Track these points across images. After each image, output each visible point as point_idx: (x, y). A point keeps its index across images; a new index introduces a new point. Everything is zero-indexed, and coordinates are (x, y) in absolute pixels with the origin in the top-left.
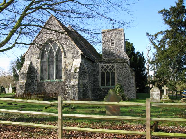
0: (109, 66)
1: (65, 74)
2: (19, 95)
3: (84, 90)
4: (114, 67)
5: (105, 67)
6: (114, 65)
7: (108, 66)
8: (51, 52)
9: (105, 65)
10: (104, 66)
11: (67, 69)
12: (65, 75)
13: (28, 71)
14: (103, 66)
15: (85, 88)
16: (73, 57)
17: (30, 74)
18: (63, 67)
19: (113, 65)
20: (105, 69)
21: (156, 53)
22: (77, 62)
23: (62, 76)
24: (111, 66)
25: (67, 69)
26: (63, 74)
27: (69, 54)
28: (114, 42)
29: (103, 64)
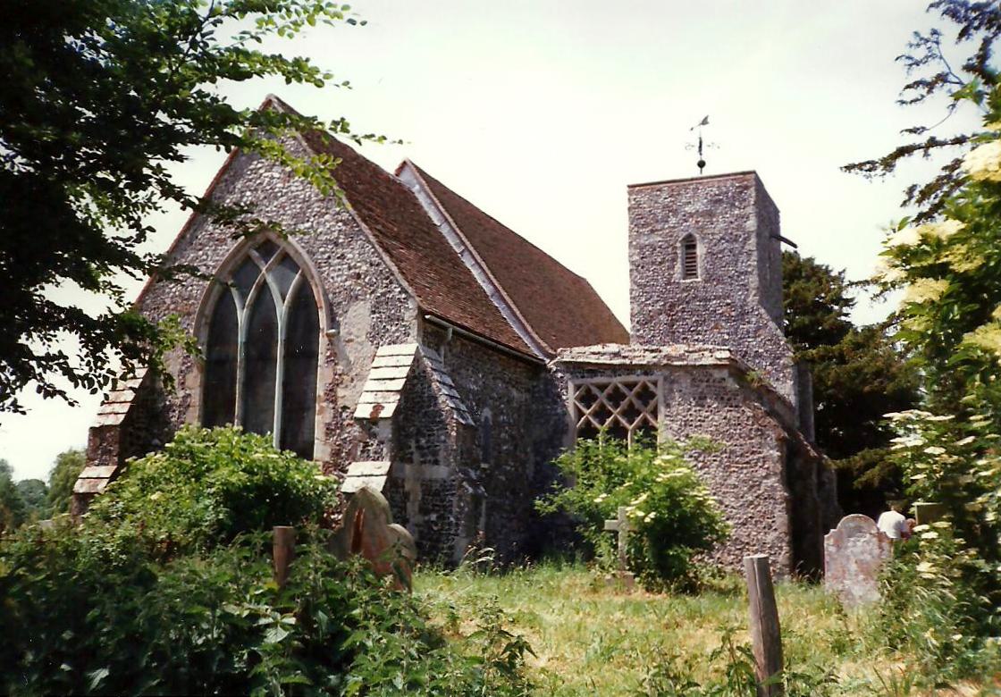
0: (624, 390)
1: (329, 431)
2: (175, 650)
3: (429, 523)
4: (653, 395)
5: (631, 396)
6: (655, 384)
7: (616, 389)
8: (262, 303)
9: (602, 387)
10: (595, 391)
11: (340, 403)
12: (327, 434)
13: (128, 414)
14: (588, 391)
15: (434, 517)
16: (376, 336)
17: (143, 434)
18: (320, 391)
19: (645, 387)
20: (631, 405)
21: (846, 315)
22: (393, 361)
23: (312, 444)
24: (636, 389)
25: (340, 403)
26: (319, 432)
27: (357, 318)
28: (700, 250)
29: (589, 381)
